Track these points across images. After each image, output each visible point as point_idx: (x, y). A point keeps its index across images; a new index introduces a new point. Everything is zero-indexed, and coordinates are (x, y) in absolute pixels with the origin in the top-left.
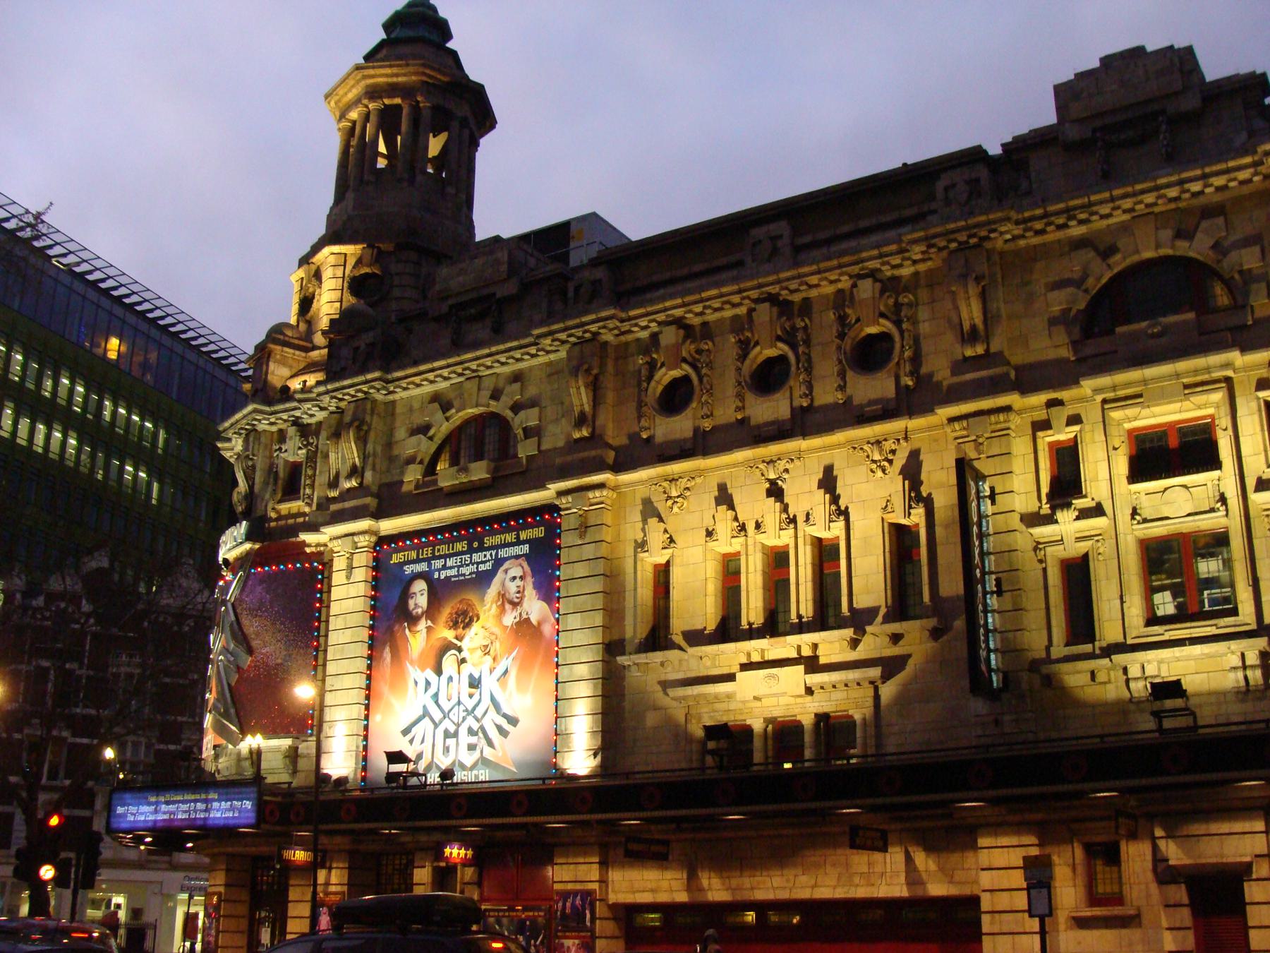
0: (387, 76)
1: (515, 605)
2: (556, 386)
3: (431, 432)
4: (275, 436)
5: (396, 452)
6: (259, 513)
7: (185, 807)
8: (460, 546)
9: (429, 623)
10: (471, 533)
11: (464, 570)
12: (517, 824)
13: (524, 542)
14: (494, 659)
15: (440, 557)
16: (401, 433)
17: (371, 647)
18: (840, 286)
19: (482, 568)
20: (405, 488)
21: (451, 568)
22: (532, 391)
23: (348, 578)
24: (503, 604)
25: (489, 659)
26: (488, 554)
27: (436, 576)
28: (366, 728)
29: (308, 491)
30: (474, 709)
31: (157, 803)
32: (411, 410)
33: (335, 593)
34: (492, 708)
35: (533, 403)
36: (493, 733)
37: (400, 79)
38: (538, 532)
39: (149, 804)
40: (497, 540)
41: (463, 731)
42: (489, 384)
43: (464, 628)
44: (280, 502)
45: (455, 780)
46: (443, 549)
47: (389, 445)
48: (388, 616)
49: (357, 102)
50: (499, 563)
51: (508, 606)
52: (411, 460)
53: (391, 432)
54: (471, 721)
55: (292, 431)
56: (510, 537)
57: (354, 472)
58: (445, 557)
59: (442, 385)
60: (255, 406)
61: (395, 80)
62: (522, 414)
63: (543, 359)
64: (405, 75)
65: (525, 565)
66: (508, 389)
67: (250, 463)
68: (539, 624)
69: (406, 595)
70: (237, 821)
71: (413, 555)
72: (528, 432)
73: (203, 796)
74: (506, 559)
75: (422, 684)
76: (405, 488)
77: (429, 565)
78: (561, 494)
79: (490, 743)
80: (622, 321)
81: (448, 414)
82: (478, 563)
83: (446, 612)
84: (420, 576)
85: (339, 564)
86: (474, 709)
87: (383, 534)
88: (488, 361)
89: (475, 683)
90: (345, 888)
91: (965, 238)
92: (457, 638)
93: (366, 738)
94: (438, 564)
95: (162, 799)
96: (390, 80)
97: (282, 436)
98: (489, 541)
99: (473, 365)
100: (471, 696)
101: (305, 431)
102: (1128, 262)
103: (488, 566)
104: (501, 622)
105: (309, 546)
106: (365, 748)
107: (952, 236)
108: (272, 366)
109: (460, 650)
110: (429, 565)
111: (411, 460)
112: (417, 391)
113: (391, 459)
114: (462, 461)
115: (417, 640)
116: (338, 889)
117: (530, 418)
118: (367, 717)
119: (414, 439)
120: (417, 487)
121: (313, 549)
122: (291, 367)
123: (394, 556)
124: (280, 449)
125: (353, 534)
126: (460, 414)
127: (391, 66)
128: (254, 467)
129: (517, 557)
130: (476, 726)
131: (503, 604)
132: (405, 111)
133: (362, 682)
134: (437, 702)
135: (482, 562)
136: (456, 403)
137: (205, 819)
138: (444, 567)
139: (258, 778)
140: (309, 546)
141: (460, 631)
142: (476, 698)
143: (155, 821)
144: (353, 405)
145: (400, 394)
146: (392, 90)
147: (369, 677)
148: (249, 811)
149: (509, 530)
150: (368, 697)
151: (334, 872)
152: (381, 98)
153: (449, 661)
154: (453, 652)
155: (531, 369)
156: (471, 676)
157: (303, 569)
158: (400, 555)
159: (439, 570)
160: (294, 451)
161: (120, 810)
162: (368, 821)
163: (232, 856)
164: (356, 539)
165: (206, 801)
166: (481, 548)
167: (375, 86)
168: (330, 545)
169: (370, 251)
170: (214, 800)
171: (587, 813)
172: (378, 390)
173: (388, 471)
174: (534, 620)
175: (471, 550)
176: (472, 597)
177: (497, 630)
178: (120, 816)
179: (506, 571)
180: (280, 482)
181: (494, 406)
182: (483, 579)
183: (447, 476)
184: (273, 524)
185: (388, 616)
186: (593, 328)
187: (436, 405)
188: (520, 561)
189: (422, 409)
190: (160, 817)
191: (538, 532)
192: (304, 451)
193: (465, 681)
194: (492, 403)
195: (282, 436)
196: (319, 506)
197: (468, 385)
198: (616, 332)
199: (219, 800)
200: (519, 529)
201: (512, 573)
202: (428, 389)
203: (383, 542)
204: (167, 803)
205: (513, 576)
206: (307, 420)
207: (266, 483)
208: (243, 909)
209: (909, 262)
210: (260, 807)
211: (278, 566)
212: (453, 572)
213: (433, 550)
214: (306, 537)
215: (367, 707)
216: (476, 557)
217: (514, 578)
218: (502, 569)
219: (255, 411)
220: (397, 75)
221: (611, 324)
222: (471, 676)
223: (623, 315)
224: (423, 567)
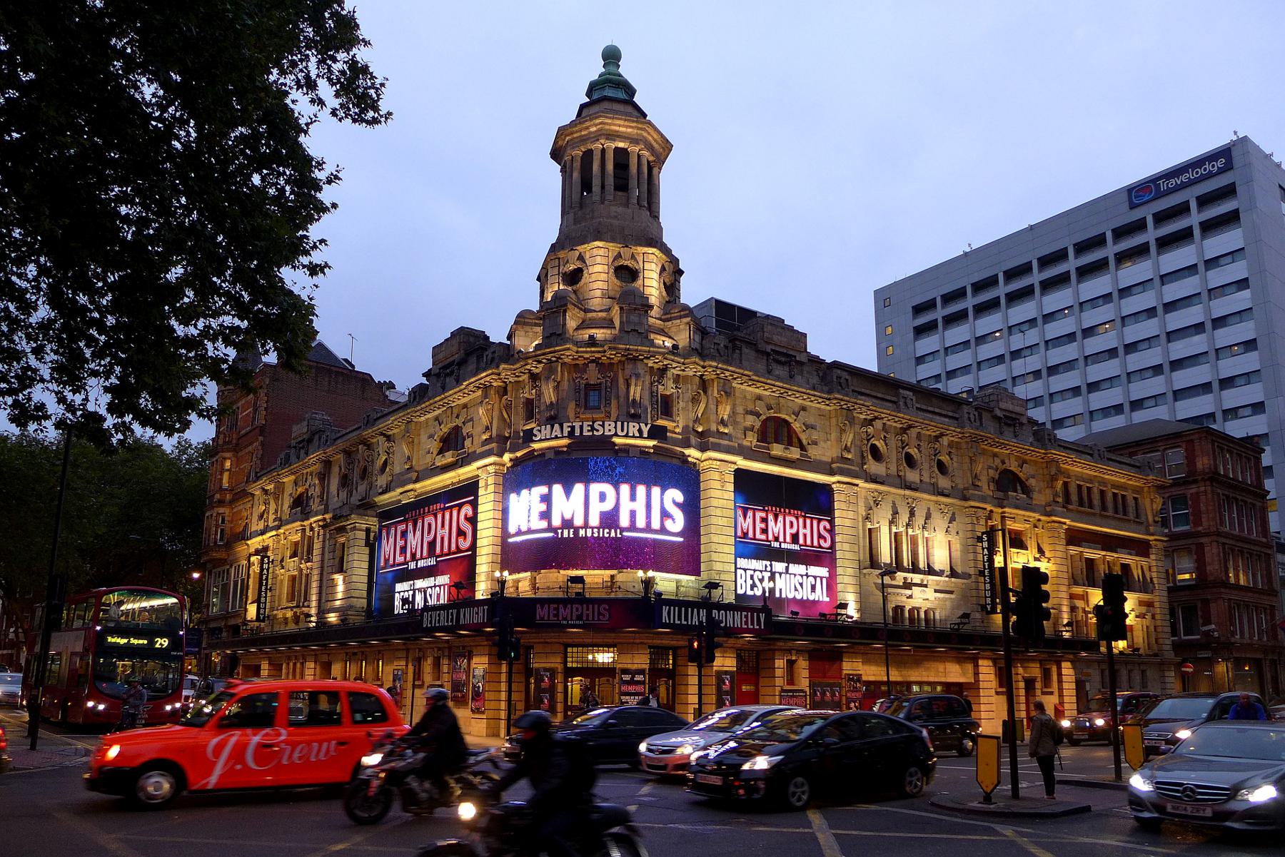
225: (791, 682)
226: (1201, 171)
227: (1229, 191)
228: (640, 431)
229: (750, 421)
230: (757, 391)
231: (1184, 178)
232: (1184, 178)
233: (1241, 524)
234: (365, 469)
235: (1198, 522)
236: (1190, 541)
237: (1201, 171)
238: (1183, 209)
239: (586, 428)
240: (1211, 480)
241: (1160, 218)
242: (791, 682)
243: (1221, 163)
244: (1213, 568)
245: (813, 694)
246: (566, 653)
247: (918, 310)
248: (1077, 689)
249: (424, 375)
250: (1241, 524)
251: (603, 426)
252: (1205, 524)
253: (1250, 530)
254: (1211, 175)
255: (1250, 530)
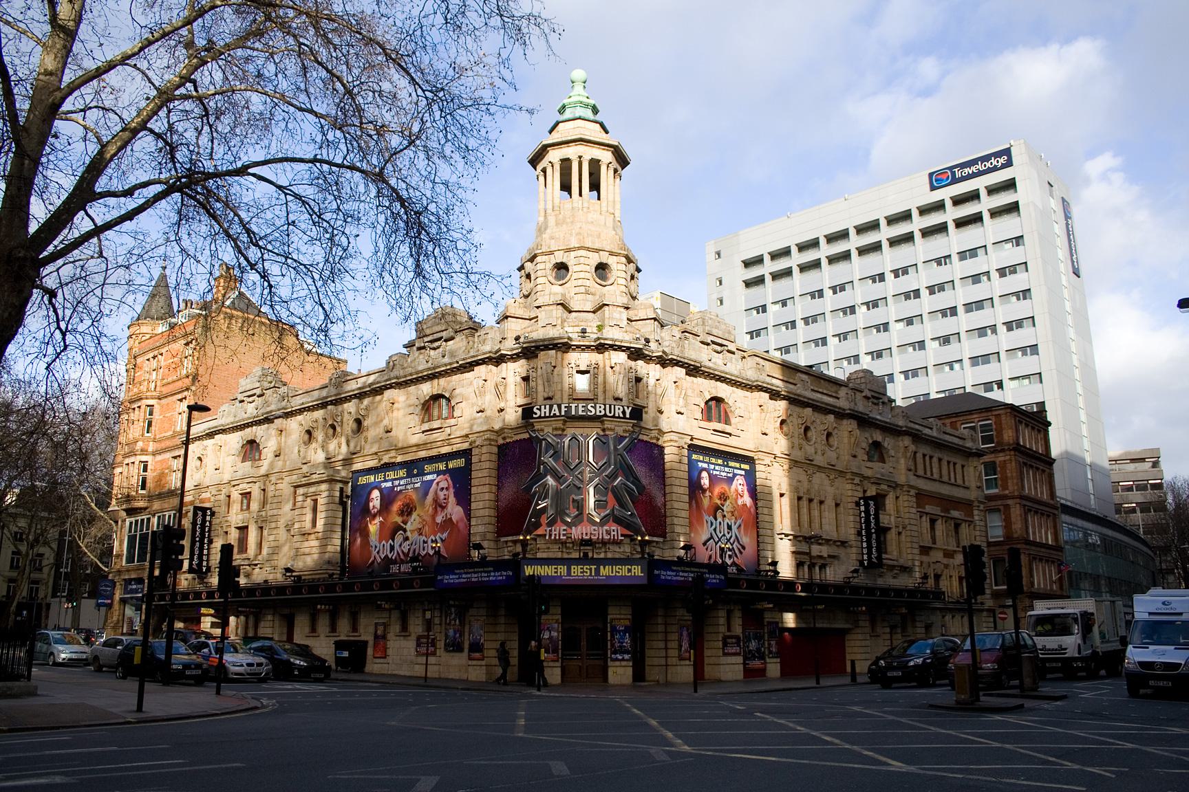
50: (735, 475)
84: (705, 469)
89: (729, 527)
98: (732, 464)
109: (405, 531)
153: (719, 514)
191: (747, 467)
225: (729, 630)
226: (988, 165)
227: (1010, 185)
228: (624, 412)
231: (974, 169)
232: (974, 169)
233: (1036, 488)
234: (358, 422)
235: (1005, 487)
236: (999, 502)
237: (988, 165)
238: (974, 196)
239: (581, 409)
240: (1015, 449)
241: (958, 201)
242: (729, 630)
243: (1002, 160)
244: (1017, 526)
245: (731, 637)
247: (748, 264)
248: (499, 454)
249: (405, 346)
250: (1036, 488)
251: (595, 408)
252: (1011, 488)
253: (1042, 493)
254: (995, 169)
255: (1042, 493)
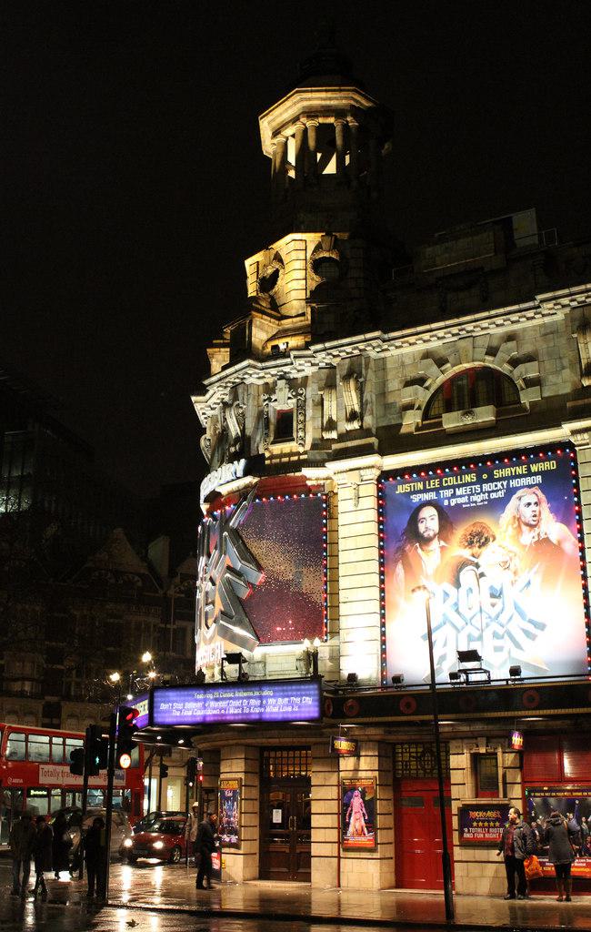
0: (322, 99)
1: (532, 527)
2: (552, 344)
3: (427, 384)
4: (261, 388)
5: (391, 399)
6: (253, 453)
7: (237, 703)
8: (468, 478)
9: (442, 543)
10: (482, 466)
11: (475, 498)
12: (496, 718)
13: (536, 474)
14: (515, 573)
15: (448, 487)
16: (394, 384)
17: (382, 565)
18: (266, 380)
19: (494, 496)
20: (403, 430)
21: (461, 496)
22: (527, 348)
23: (356, 505)
24: (519, 526)
25: (509, 574)
26: (499, 484)
27: (446, 503)
28: (383, 634)
29: (301, 434)
30: (498, 616)
31: (205, 700)
32: (403, 364)
33: (342, 519)
34: (516, 614)
35: (530, 358)
36: (520, 637)
37: (332, 103)
38: (551, 465)
39: (197, 701)
40: (507, 472)
41: (488, 634)
42: (483, 343)
43: (480, 547)
44: (273, 443)
45: (523, 675)
46: (452, 481)
47: (383, 394)
48: (397, 535)
49: (295, 120)
50: (510, 492)
51: (525, 528)
52: (410, 407)
53: (384, 383)
54: (495, 627)
55: (281, 383)
56: (520, 470)
57: (353, 417)
58: (454, 487)
59: (435, 344)
60: (251, 362)
61: (328, 103)
62: (521, 367)
63: (539, 321)
64: (336, 99)
65: (539, 492)
66: (504, 347)
67: (241, 411)
68: (559, 542)
69: (414, 519)
70: (294, 715)
71: (420, 486)
72: (530, 383)
73: (257, 694)
74: (516, 489)
75: (440, 595)
76: (403, 430)
77: (438, 494)
78: (574, 432)
79: (518, 646)
80: (384, 341)
81: (443, 368)
82: (489, 492)
83: (460, 532)
84: (429, 503)
85: (343, 494)
86: (498, 616)
87: (385, 469)
88: (485, 324)
89: (496, 595)
90: (377, 774)
91: (583, 299)
92: (473, 556)
93: (383, 643)
94: (448, 493)
95: (210, 696)
96: (324, 103)
97: (270, 389)
98: (497, 474)
99: (469, 327)
100: (493, 605)
101: (293, 384)
102: (457, 369)
103: (501, 494)
104: (519, 542)
105: (309, 479)
106: (384, 652)
107: (342, 348)
108: (254, 330)
109: (477, 566)
110: (438, 494)
111: (410, 407)
112: (407, 350)
113: (387, 407)
114: (467, 405)
115: (432, 559)
116: (369, 774)
117: (531, 371)
118: (383, 625)
119: (410, 389)
120: (418, 429)
121: (314, 483)
122: (267, 332)
123: (400, 487)
124: (270, 399)
125: (359, 469)
126: (455, 368)
127: (326, 91)
128: (243, 415)
129: (530, 486)
130: (501, 631)
131: (519, 526)
132: (338, 130)
133: (376, 593)
134: (457, 611)
135: (493, 491)
136: (451, 359)
137: (260, 713)
138: (454, 495)
139: (316, 678)
140: (309, 479)
141: (476, 550)
142: (498, 608)
143: (205, 716)
144: (348, 360)
145: (393, 352)
146: (326, 111)
147: (382, 590)
148: (310, 706)
149: (520, 464)
150: (383, 607)
151: (362, 759)
152: (317, 117)
153: (467, 576)
154: (471, 567)
155: (524, 330)
156: (491, 588)
157: (307, 500)
158: (406, 486)
159: (449, 499)
160: (283, 401)
161: (163, 706)
162: (377, 716)
163: (247, 746)
164: (362, 472)
165: (261, 698)
166: (491, 479)
167: (310, 107)
168: (335, 477)
169: (328, 239)
170: (267, 697)
171: (534, 709)
172: (251, 375)
173: (385, 415)
174: (554, 539)
175: (480, 481)
176: (486, 520)
177: (516, 549)
178: (165, 712)
179: (520, 499)
180: (272, 428)
181: (490, 362)
182: (497, 505)
183: (451, 422)
184: (267, 462)
185: (397, 535)
186: (361, 346)
187: (430, 361)
188: (533, 489)
189: (414, 364)
190: (209, 712)
191: (551, 465)
192: (294, 400)
193: (486, 592)
194: (489, 358)
195: (270, 389)
196: (314, 446)
197: (463, 344)
198: (379, 350)
199: (274, 697)
200: (529, 463)
201: (526, 500)
202: (421, 347)
203: (385, 475)
204: (217, 700)
205: (528, 501)
206: (294, 374)
207: (256, 428)
208: (255, 793)
209: (393, 348)
210: (322, 702)
211: (283, 496)
212: (465, 500)
213: (441, 482)
214: (306, 472)
215: (383, 616)
216: (486, 487)
217: (529, 504)
218: (514, 497)
219: (249, 366)
220: (330, 99)
221: (374, 343)
222: (491, 588)
223: (386, 336)
224: (432, 496)
229: (408, 395)
230: (534, 322)
246: (395, 753)
